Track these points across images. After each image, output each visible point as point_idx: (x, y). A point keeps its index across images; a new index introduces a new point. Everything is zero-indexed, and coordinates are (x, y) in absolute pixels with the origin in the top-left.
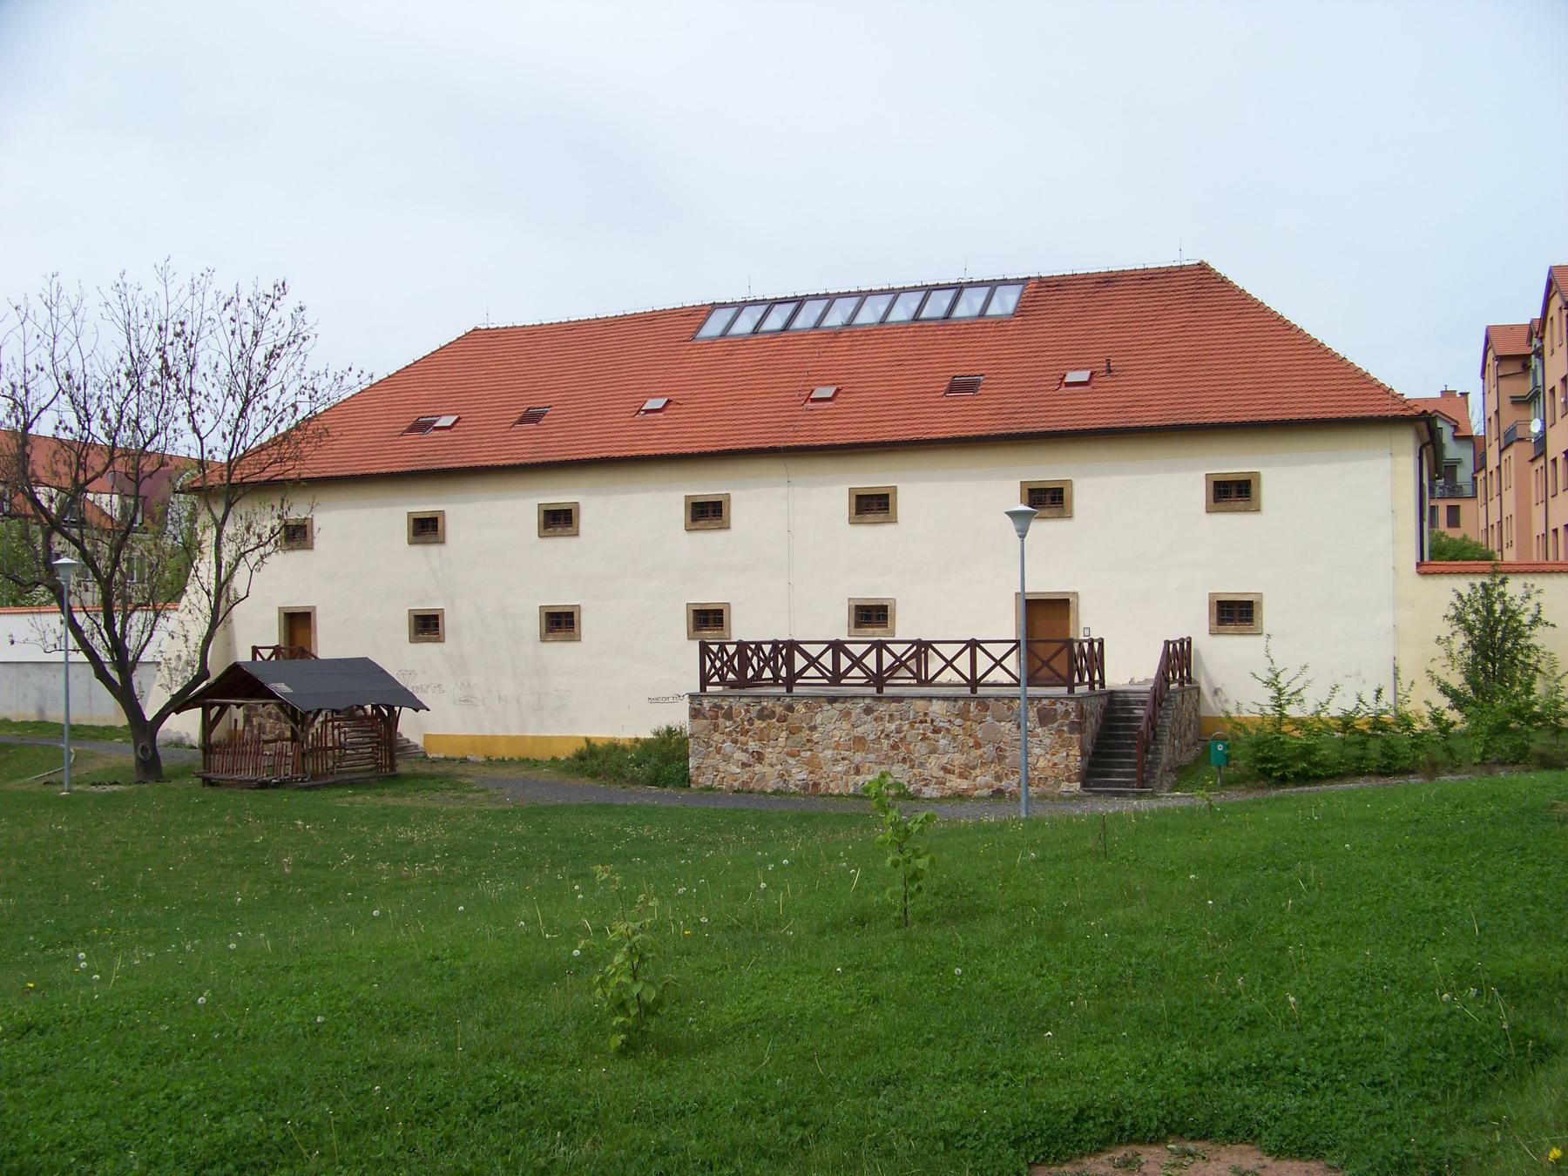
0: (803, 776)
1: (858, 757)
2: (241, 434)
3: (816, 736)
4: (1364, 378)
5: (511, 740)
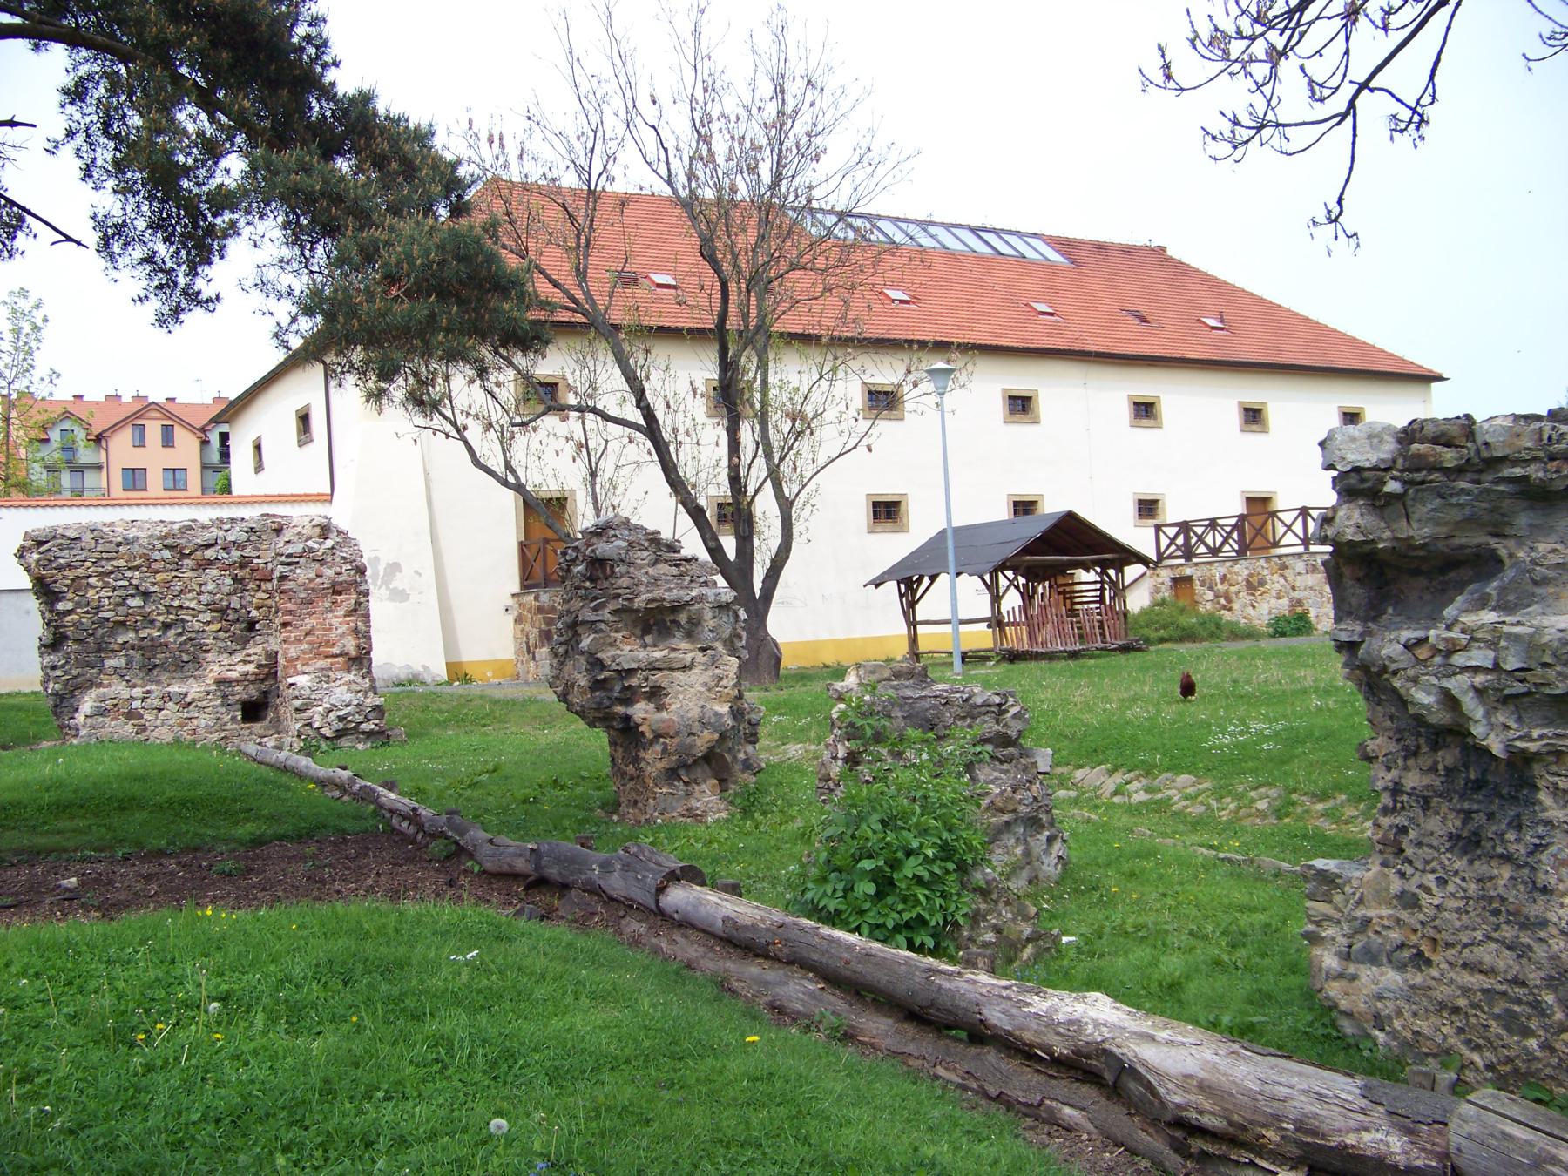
5: (838, 644)
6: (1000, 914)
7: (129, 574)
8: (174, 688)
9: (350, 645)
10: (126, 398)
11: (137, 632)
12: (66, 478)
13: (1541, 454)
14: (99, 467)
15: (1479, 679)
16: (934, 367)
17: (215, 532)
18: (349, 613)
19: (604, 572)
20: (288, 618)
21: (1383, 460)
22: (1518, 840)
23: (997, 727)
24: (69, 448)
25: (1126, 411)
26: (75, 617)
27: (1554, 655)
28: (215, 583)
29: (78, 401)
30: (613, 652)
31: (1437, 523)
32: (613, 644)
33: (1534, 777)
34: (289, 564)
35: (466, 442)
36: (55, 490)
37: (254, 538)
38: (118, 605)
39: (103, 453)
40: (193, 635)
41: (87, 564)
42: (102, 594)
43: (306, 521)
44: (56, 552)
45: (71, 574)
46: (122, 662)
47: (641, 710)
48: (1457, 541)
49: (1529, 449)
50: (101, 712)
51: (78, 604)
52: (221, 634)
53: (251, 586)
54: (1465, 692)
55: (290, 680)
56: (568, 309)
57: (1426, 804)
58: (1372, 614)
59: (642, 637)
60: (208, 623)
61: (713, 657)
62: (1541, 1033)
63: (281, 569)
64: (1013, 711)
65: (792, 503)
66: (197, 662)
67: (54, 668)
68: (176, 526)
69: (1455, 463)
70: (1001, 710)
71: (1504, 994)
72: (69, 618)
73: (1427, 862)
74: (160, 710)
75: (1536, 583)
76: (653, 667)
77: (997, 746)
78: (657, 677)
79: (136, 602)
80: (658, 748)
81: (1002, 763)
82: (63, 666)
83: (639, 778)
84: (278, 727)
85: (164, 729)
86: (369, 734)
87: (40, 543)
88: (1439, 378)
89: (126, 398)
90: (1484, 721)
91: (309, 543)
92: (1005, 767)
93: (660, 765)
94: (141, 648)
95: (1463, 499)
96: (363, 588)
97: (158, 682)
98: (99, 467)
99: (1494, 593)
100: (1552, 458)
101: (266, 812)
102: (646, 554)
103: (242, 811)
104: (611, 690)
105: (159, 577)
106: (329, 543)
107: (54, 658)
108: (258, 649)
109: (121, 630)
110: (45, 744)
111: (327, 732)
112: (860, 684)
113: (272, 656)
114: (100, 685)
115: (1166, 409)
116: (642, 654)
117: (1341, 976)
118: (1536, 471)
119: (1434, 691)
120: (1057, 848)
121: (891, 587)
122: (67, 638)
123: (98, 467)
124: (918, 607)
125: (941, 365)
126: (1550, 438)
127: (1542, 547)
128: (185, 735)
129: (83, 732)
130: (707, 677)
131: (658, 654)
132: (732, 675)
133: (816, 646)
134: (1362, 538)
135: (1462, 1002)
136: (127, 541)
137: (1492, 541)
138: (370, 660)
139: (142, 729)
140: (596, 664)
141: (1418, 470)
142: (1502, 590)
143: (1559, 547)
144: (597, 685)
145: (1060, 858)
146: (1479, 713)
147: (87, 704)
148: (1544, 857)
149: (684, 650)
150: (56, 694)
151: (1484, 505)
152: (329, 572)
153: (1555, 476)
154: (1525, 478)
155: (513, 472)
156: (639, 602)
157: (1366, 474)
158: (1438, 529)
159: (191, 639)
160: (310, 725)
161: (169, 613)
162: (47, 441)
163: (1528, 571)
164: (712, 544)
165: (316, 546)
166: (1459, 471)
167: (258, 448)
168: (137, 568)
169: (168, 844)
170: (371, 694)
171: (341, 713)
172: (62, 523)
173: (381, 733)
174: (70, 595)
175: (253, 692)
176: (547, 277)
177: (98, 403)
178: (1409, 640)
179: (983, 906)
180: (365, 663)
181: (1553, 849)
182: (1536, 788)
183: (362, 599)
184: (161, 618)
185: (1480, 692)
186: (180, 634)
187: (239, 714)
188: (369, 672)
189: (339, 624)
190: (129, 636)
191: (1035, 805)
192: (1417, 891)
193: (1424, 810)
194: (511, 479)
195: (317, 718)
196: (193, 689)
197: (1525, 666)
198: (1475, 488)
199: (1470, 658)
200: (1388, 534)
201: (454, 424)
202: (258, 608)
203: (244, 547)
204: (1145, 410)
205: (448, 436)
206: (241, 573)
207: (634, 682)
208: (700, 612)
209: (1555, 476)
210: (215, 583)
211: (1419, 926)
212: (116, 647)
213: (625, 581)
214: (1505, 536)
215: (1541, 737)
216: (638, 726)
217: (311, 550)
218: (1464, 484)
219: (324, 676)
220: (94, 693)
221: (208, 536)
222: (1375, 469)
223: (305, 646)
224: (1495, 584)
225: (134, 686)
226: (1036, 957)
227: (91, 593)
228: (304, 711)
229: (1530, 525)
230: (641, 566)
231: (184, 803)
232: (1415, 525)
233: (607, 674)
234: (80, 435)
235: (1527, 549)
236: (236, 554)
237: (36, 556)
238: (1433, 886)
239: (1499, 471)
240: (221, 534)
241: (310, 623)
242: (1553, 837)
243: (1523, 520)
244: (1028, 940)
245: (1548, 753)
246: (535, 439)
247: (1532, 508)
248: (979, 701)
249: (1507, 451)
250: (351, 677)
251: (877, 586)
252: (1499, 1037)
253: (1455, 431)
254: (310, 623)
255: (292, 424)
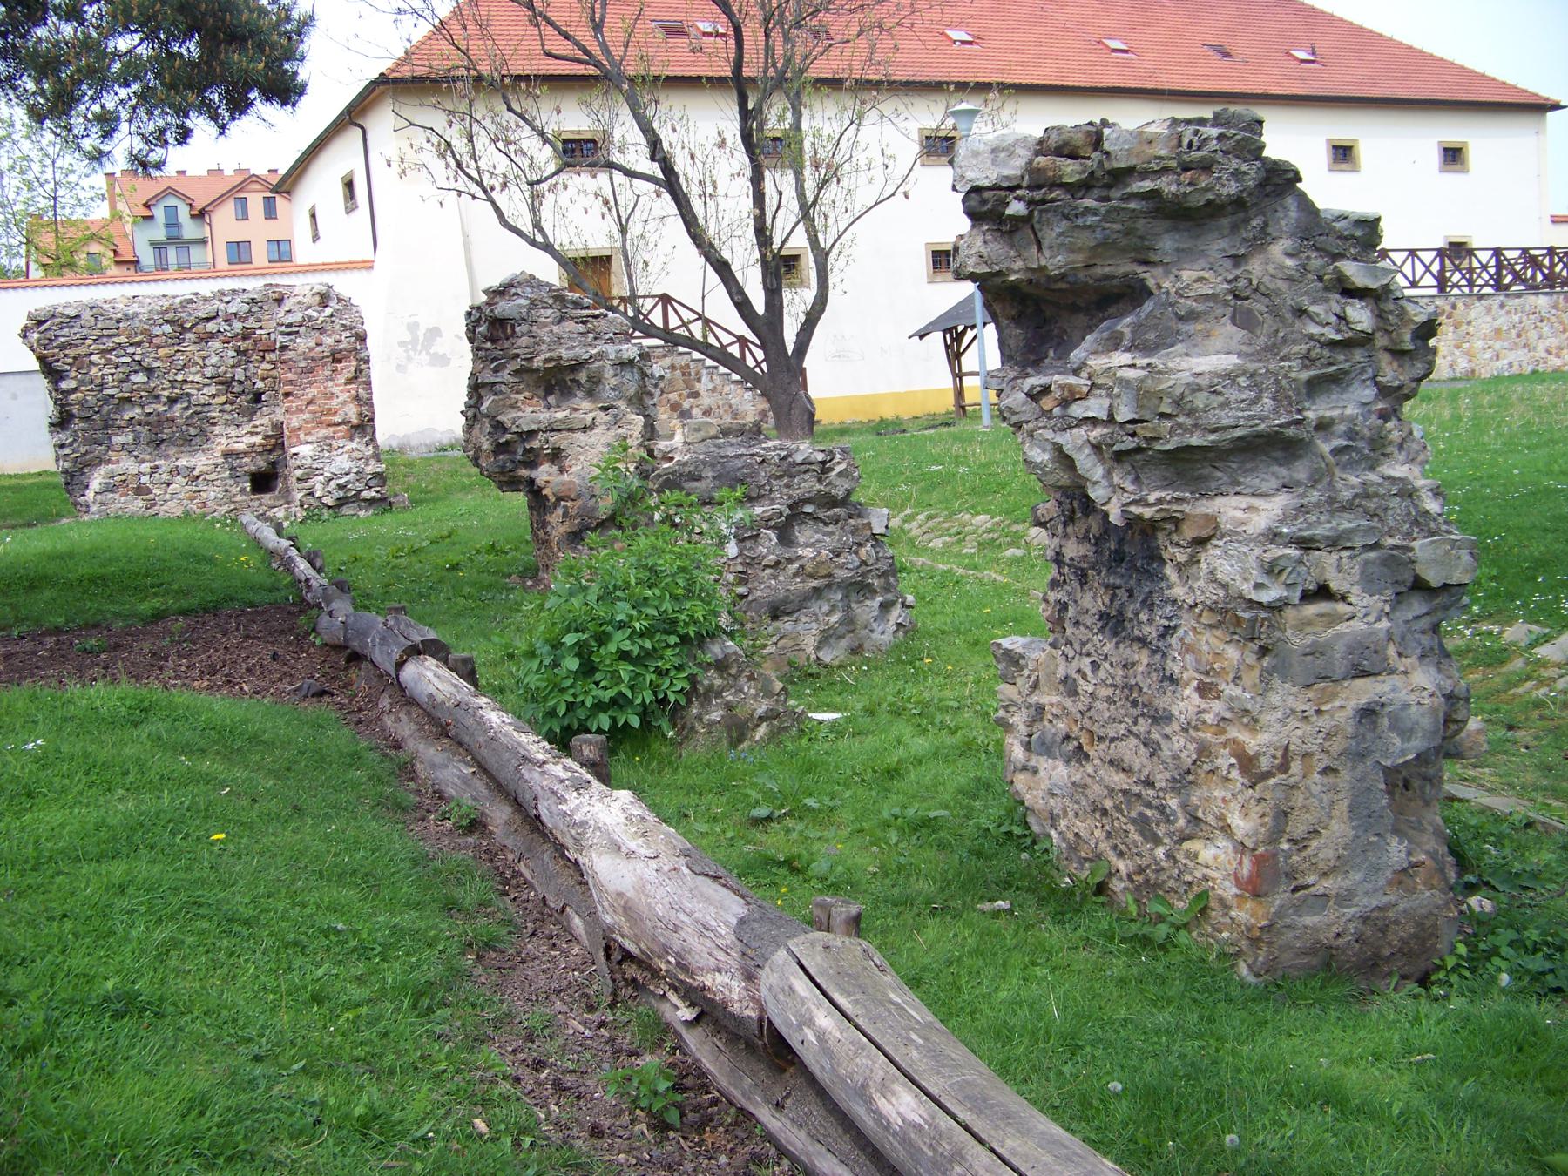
0: (1465, 365)
1: (1497, 345)
2: (703, 195)
3: (1471, 329)
4: (1472, 73)
5: (897, 396)
6: (741, 690)
7: (131, 350)
8: (183, 462)
9: (352, 412)
10: (229, 172)
11: (142, 407)
12: (172, 253)
13: (1173, 164)
14: (203, 242)
15: (1097, 433)
16: (958, 108)
17: (217, 304)
18: (350, 381)
19: (504, 331)
20: (288, 388)
21: (1007, 178)
22: (1150, 621)
23: (818, 487)
24: (172, 224)
25: (1435, 157)
26: (80, 395)
27: (1177, 403)
28: (218, 356)
29: (181, 177)
30: (513, 414)
31: (1071, 250)
32: (514, 406)
33: (1158, 547)
34: (289, 334)
35: (493, 203)
36: (162, 267)
37: (255, 309)
38: (122, 381)
39: (207, 228)
40: (199, 409)
41: (88, 342)
42: (106, 371)
43: (306, 290)
44: (55, 330)
45: (72, 352)
46: (130, 438)
47: (544, 473)
48: (1099, 271)
49: (1161, 158)
50: (110, 488)
51: (82, 383)
52: (228, 407)
53: (255, 357)
54: (1080, 449)
55: (293, 450)
56: (579, 61)
57: (1083, 578)
58: (1032, 358)
59: (545, 398)
60: (214, 396)
61: (616, 416)
62: (1166, 840)
63: (281, 339)
64: (839, 469)
65: (827, 254)
66: (205, 436)
67: (62, 446)
68: (178, 300)
69: (1077, 177)
70: (825, 467)
71: (1139, 796)
72: (73, 396)
73: (1083, 644)
74: (169, 484)
75: (1181, 318)
76: (553, 429)
77: (820, 506)
78: (557, 439)
79: (139, 378)
80: (560, 511)
81: (826, 524)
82: (71, 444)
83: (545, 543)
84: (287, 499)
85: (174, 503)
86: (371, 502)
87: (41, 323)
88: (1556, 106)
89: (229, 172)
90: (1105, 483)
91: (310, 312)
92: (831, 528)
93: (562, 529)
94: (147, 424)
95: (1091, 219)
96: (363, 355)
97: (166, 457)
98: (203, 242)
99: (1127, 331)
100: (1186, 169)
101: (175, 587)
102: (549, 311)
103: (152, 586)
104: (515, 453)
105: (161, 352)
106: (328, 311)
107: (64, 437)
108: (265, 421)
109: (127, 406)
110: (65, 521)
111: (328, 501)
112: (686, 443)
113: (278, 427)
114: (109, 462)
115: (1364, 153)
116: (544, 416)
117: (1024, 768)
118: (1169, 184)
119: (1049, 447)
120: (896, 614)
121: (937, 339)
122: (73, 416)
123: (203, 242)
124: (963, 359)
125: (964, 106)
126: (1190, 145)
127: (1187, 275)
128: (195, 509)
129: (93, 509)
130: (609, 437)
131: (560, 415)
132: (636, 434)
133: (874, 399)
134: (987, 270)
135: (1108, 804)
136: (127, 318)
137: (1140, 269)
138: (373, 428)
139: (152, 504)
140: (499, 427)
141: (1039, 187)
142: (1138, 328)
143: (1206, 275)
144: (500, 448)
145: (900, 625)
146: (1098, 472)
147: (97, 480)
148: (1174, 641)
149: (585, 409)
150: (65, 472)
151: (1117, 227)
152: (329, 341)
153: (1189, 189)
154: (1154, 194)
155: (541, 230)
156: (538, 363)
157: (987, 195)
158: (1072, 257)
159: (197, 413)
160: (311, 494)
161: (173, 387)
162: (152, 217)
163: (1171, 305)
164: (738, 298)
165: (315, 314)
166: (1085, 186)
167: (313, 216)
168: (138, 344)
169: (67, 622)
170: (372, 462)
171: (341, 482)
172: (63, 302)
173: (383, 500)
174: (73, 374)
175: (261, 463)
176: (557, 28)
177: (200, 178)
178: (1033, 387)
179: (718, 682)
180: (369, 430)
181: (1180, 632)
182: (1163, 562)
183: (363, 367)
184: (166, 393)
185: (1097, 448)
186: (186, 408)
187: (248, 486)
188: (373, 439)
189: (339, 392)
190: (136, 412)
191: (864, 568)
192: (1076, 676)
193: (1082, 585)
194: (539, 239)
195: (319, 486)
196: (201, 462)
197: (1136, 417)
198: (1103, 207)
199: (1088, 408)
200: (1019, 264)
201: (480, 184)
202: (263, 379)
203: (246, 319)
204: (1453, 156)
205: (474, 197)
206: (244, 345)
207: (535, 444)
208: (600, 370)
209: (1189, 189)
210: (218, 356)
211: (1079, 716)
212: (123, 423)
213: (524, 341)
214: (1154, 264)
215: (1160, 501)
216: (541, 489)
217: (310, 319)
218: (1088, 202)
219: (327, 445)
220: (103, 469)
221: (209, 309)
222: (995, 187)
223: (307, 416)
224: (1128, 320)
225: (143, 462)
226: (773, 735)
227: (94, 371)
228: (306, 481)
229: (1178, 250)
230: (545, 325)
231: (93, 581)
232: (1047, 252)
233: (508, 436)
234: (183, 213)
235: (1172, 278)
236: (238, 326)
237: (36, 336)
238: (1088, 670)
239: (1127, 185)
240: (222, 306)
241: (311, 392)
242: (1180, 618)
243: (1167, 244)
244: (761, 719)
245: (1164, 519)
246: (563, 197)
247: (1175, 229)
248: (799, 458)
249: (1133, 162)
250: (354, 445)
251: (921, 337)
252: (1134, 842)
253: (1079, 140)
254: (311, 392)
255: (339, 190)
